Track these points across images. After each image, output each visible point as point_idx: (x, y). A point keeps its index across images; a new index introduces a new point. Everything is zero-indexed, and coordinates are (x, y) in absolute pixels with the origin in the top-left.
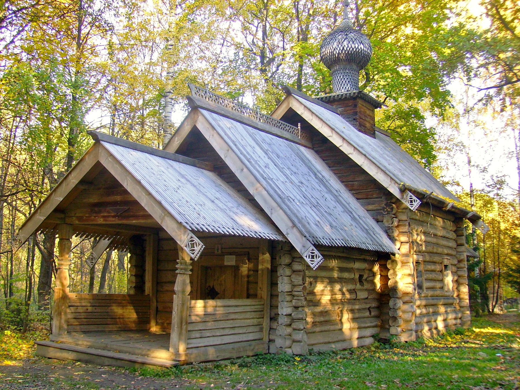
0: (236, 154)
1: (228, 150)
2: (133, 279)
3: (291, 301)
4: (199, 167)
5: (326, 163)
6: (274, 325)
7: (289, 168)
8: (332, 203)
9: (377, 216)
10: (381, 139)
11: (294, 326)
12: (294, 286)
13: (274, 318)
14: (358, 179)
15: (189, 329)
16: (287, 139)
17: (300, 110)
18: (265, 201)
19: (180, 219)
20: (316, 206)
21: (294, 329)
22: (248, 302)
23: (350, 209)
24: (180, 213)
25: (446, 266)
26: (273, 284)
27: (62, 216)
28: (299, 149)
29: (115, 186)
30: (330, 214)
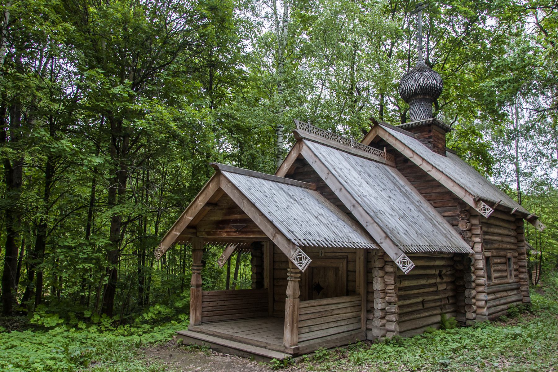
0: (335, 177)
1: (328, 174)
2: (255, 276)
3: (385, 298)
4: (304, 188)
5: (408, 179)
6: (371, 317)
7: (379, 185)
8: (415, 213)
9: (452, 221)
10: (450, 157)
11: (388, 318)
12: (387, 285)
13: (370, 311)
14: (435, 191)
15: (300, 326)
16: (376, 161)
17: (385, 137)
18: (361, 216)
19: (289, 236)
20: (403, 217)
21: (388, 321)
22: (347, 299)
23: (430, 217)
24: (289, 231)
25: (509, 259)
26: (369, 283)
27: (194, 231)
28: (385, 169)
29: (233, 208)
30: (415, 223)
